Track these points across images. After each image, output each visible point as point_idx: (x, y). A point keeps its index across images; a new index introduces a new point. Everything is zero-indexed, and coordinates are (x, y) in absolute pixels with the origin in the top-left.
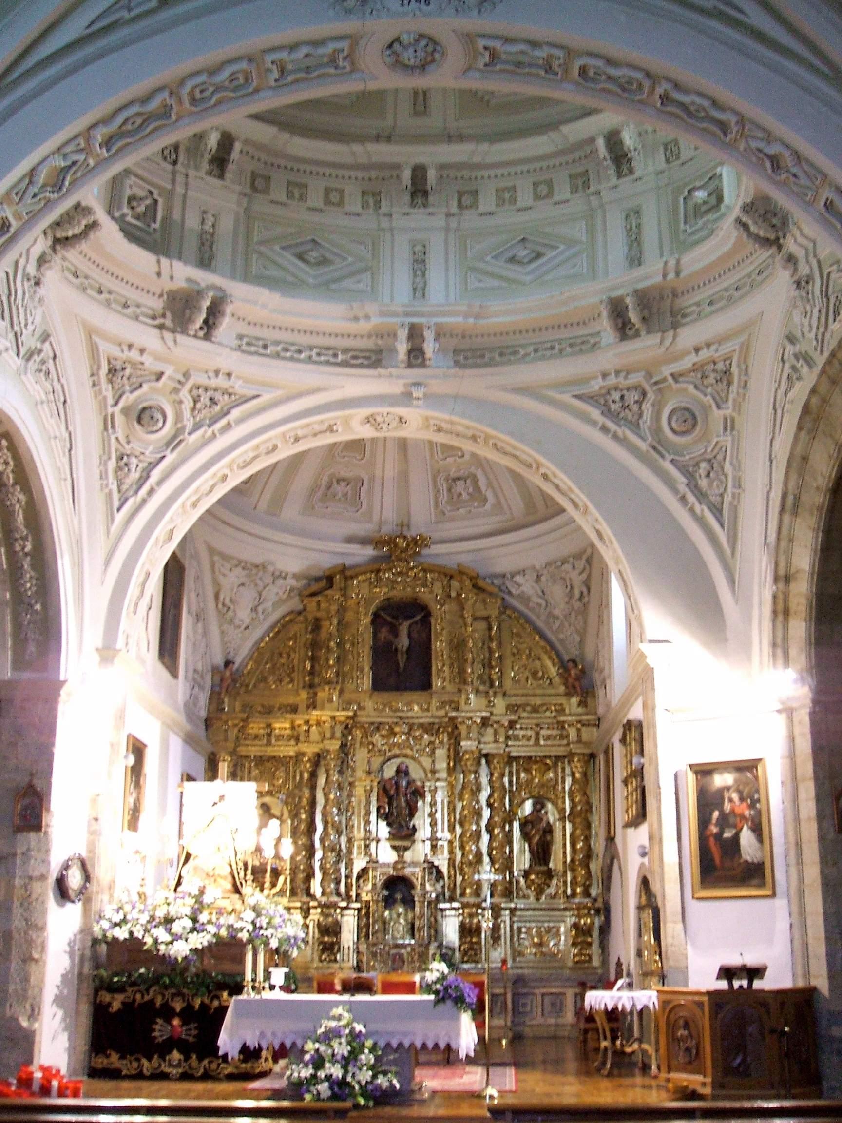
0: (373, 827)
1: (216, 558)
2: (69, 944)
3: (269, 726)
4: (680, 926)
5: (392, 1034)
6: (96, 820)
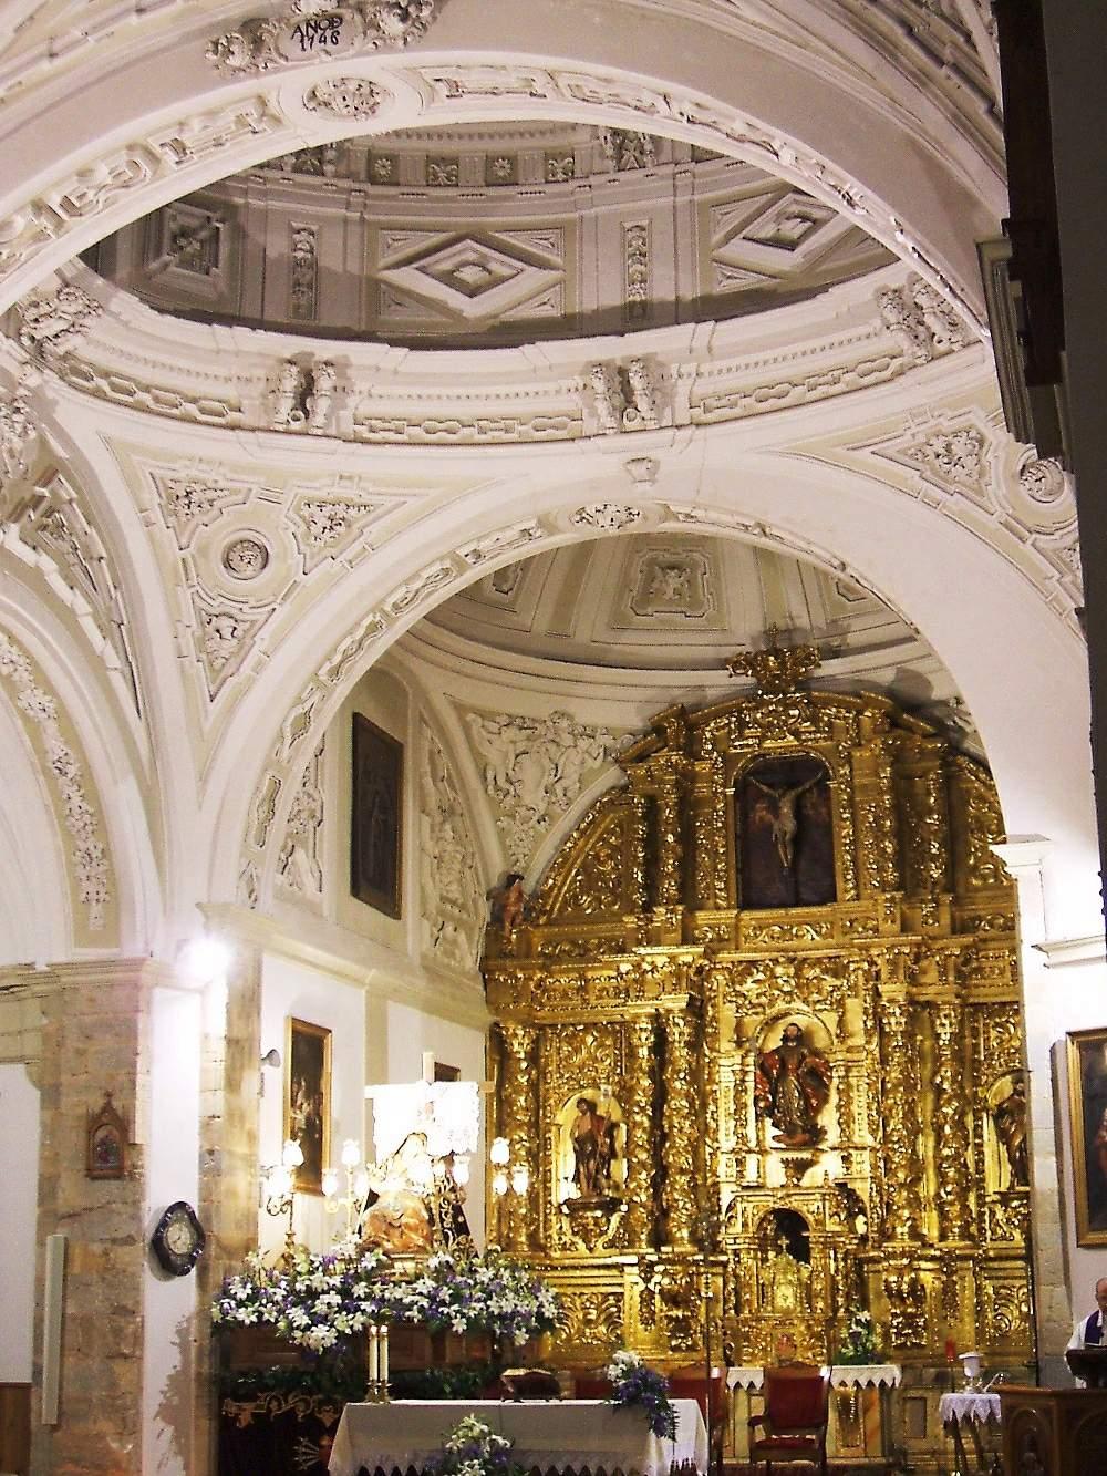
0: (751, 1131)
1: (470, 717)
2: (179, 1332)
3: (582, 977)
4: (1062, 1289)
5: (557, 1454)
6: (211, 1152)
